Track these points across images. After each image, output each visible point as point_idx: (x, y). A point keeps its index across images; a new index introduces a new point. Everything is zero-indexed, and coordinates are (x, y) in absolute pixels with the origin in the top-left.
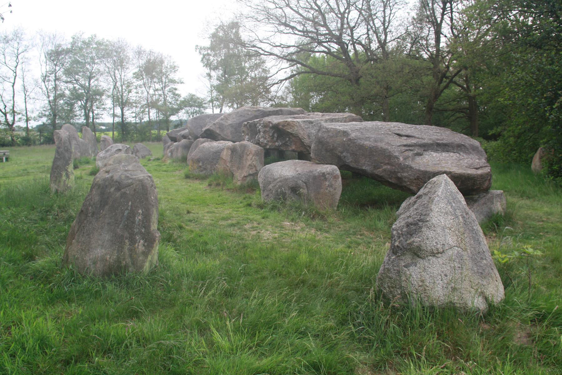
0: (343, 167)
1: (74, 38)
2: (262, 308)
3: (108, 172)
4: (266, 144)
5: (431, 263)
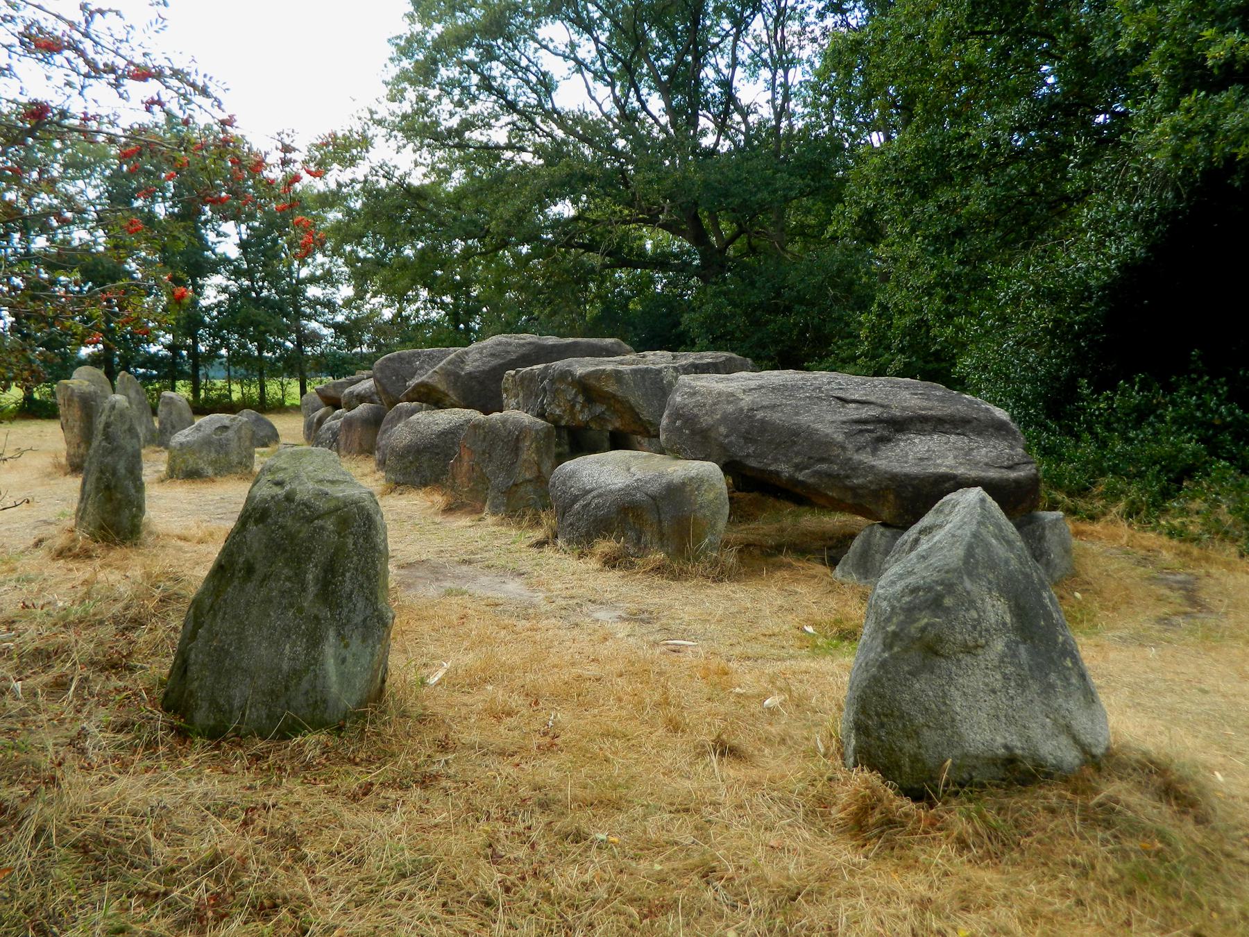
0: (731, 467)
1: (1192, 598)
2: (1130, 771)
3: (280, 484)
4: (561, 417)
5: (964, 666)
